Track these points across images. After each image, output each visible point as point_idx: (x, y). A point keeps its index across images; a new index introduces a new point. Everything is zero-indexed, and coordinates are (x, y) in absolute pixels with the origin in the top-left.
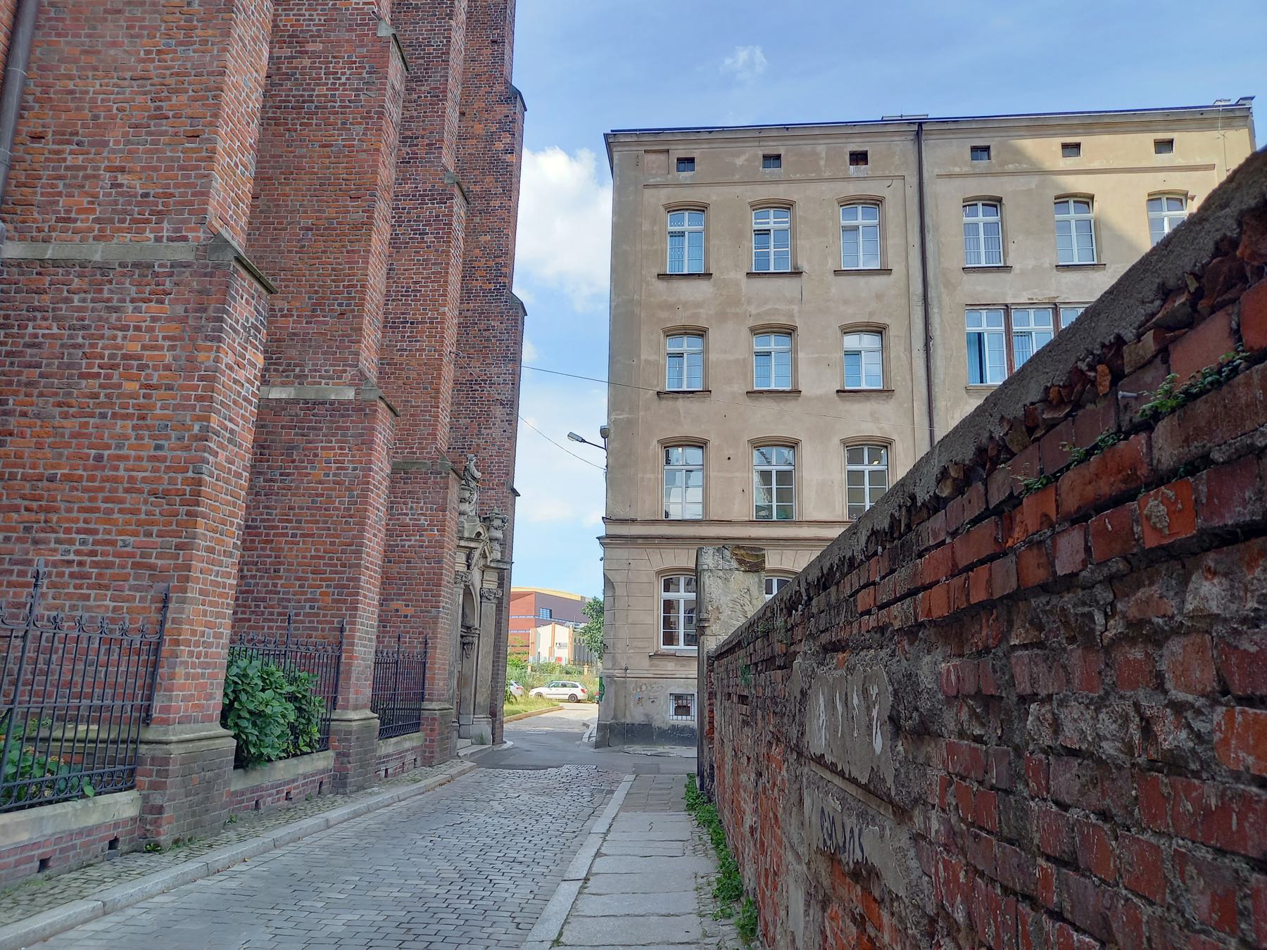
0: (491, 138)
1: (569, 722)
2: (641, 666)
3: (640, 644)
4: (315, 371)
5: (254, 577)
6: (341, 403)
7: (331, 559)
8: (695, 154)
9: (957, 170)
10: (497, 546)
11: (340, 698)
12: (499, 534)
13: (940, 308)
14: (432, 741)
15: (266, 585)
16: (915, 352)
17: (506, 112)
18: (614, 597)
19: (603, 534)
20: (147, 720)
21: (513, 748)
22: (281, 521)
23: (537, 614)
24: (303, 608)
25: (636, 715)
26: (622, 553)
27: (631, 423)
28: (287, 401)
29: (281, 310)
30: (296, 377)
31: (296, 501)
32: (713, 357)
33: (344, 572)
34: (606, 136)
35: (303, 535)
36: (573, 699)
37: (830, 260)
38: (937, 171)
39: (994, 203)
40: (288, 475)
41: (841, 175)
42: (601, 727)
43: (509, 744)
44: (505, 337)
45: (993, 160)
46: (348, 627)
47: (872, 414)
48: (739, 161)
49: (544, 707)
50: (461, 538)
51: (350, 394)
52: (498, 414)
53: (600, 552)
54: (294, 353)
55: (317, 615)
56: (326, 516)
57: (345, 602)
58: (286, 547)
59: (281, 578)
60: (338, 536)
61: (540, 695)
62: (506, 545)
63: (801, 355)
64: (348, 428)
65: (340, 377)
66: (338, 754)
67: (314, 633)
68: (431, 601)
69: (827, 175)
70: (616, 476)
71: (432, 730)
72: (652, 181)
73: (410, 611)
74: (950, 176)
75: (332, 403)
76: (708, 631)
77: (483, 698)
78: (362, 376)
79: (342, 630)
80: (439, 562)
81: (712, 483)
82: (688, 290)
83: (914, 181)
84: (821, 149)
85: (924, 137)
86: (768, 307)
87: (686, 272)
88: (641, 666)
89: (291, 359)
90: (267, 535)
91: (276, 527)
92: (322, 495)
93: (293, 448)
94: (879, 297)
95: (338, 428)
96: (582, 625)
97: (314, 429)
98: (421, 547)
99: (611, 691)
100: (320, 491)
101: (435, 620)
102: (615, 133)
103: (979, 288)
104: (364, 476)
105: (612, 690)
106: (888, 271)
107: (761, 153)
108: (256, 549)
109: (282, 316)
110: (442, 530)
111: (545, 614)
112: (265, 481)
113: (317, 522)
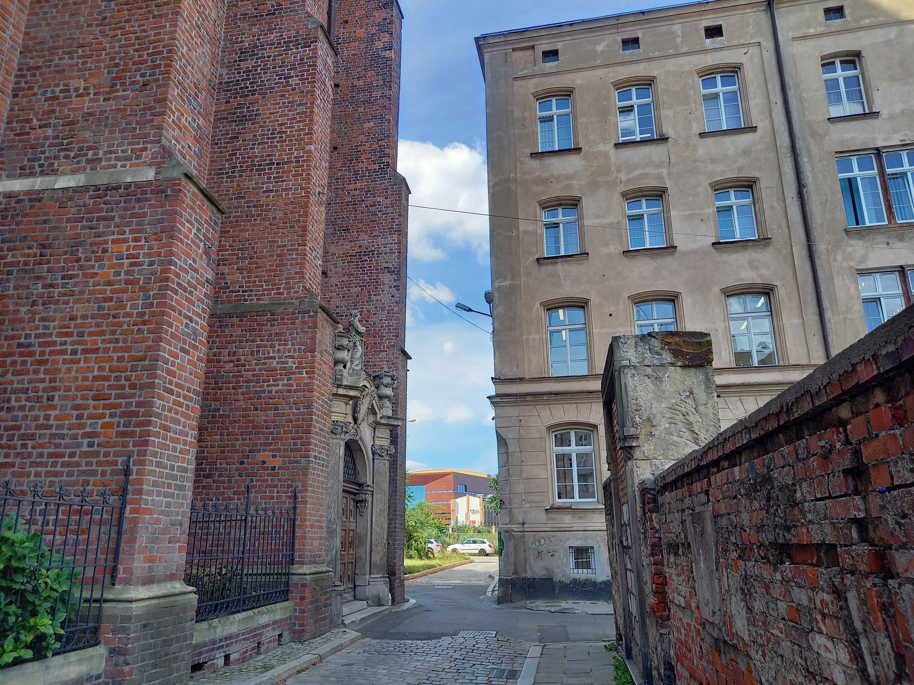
0: (371, 39)
1: (476, 575)
2: (537, 518)
3: (535, 498)
4: (111, 152)
5: (22, 408)
6: (138, 185)
7: (118, 379)
8: (559, 46)
9: (812, 31)
10: (387, 404)
11: (121, 568)
12: (389, 392)
13: (810, 157)
14: (302, 611)
15: (36, 418)
16: (788, 201)
17: (385, 16)
18: (507, 453)
19: (494, 393)
20: (292, 562)
21: (415, 607)
22: (60, 335)
24: (79, 445)
25: (536, 569)
26: (512, 411)
28: (75, 190)
29: (77, 90)
30: (89, 161)
31: (79, 309)
32: (588, 222)
33: (133, 396)
34: (477, 40)
35: (85, 351)
36: (483, 553)
37: (694, 125)
38: (792, 34)
39: (852, 59)
40: (71, 277)
41: (698, 48)
43: (413, 601)
44: (390, 210)
45: (848, 18)
46: (134, 469)
47: (750, 262)
48: (600, 48)
49: (457, 560)
50: (339, 386)
51: (150, 174)
52: (386, 281)
53: (490, 412)
54: (88, 134)
55: (97, 454)
56: (114, 324)
57: (132, 434)
58: (64, 367)
59: (54, 408)
60: (127, 349)
61: (454, 550)
62: (399, 403)
63: (673, 213)
64: (145, 215)
65: (139, 157)
66: (112, 651)
67: (92, 479)
68: (300, 450)
69: (684, 49)
70: (505, 342)
71: (302, 598)
72: (520, 74)
73: (278, 462)
74: (805, 37)
75: (128, 186)
76: (637, 454)
77: (379, 556)
78: (167, 153)
79: (127, 472)
80: (309, 406)
82: (560, 165)
83: (769, 45)
84: (677, 28)
85: (775, 6)
86: (635, 174)
87: (557, 149)
89: (84, 141)
90: (42, 353)
91: (54, 343)
92: (110, 299)
93: (78, 244)
94: (746, 153)
95: (133, 216)
96: (489, 496)
97: (104, 219)
98: (289, 391)
100: (108, 294)
101: (305, 471)
102: (484, 37)
103: (847, 136)
104: (163, 271)
105: (511, 544)
106: (753, 129)
107: (619, 38)
108: (27, 372)
109: (77, 96)
110: (311, 373)
111: (461, 488)
112: (44, 287)
113: (103, 333)
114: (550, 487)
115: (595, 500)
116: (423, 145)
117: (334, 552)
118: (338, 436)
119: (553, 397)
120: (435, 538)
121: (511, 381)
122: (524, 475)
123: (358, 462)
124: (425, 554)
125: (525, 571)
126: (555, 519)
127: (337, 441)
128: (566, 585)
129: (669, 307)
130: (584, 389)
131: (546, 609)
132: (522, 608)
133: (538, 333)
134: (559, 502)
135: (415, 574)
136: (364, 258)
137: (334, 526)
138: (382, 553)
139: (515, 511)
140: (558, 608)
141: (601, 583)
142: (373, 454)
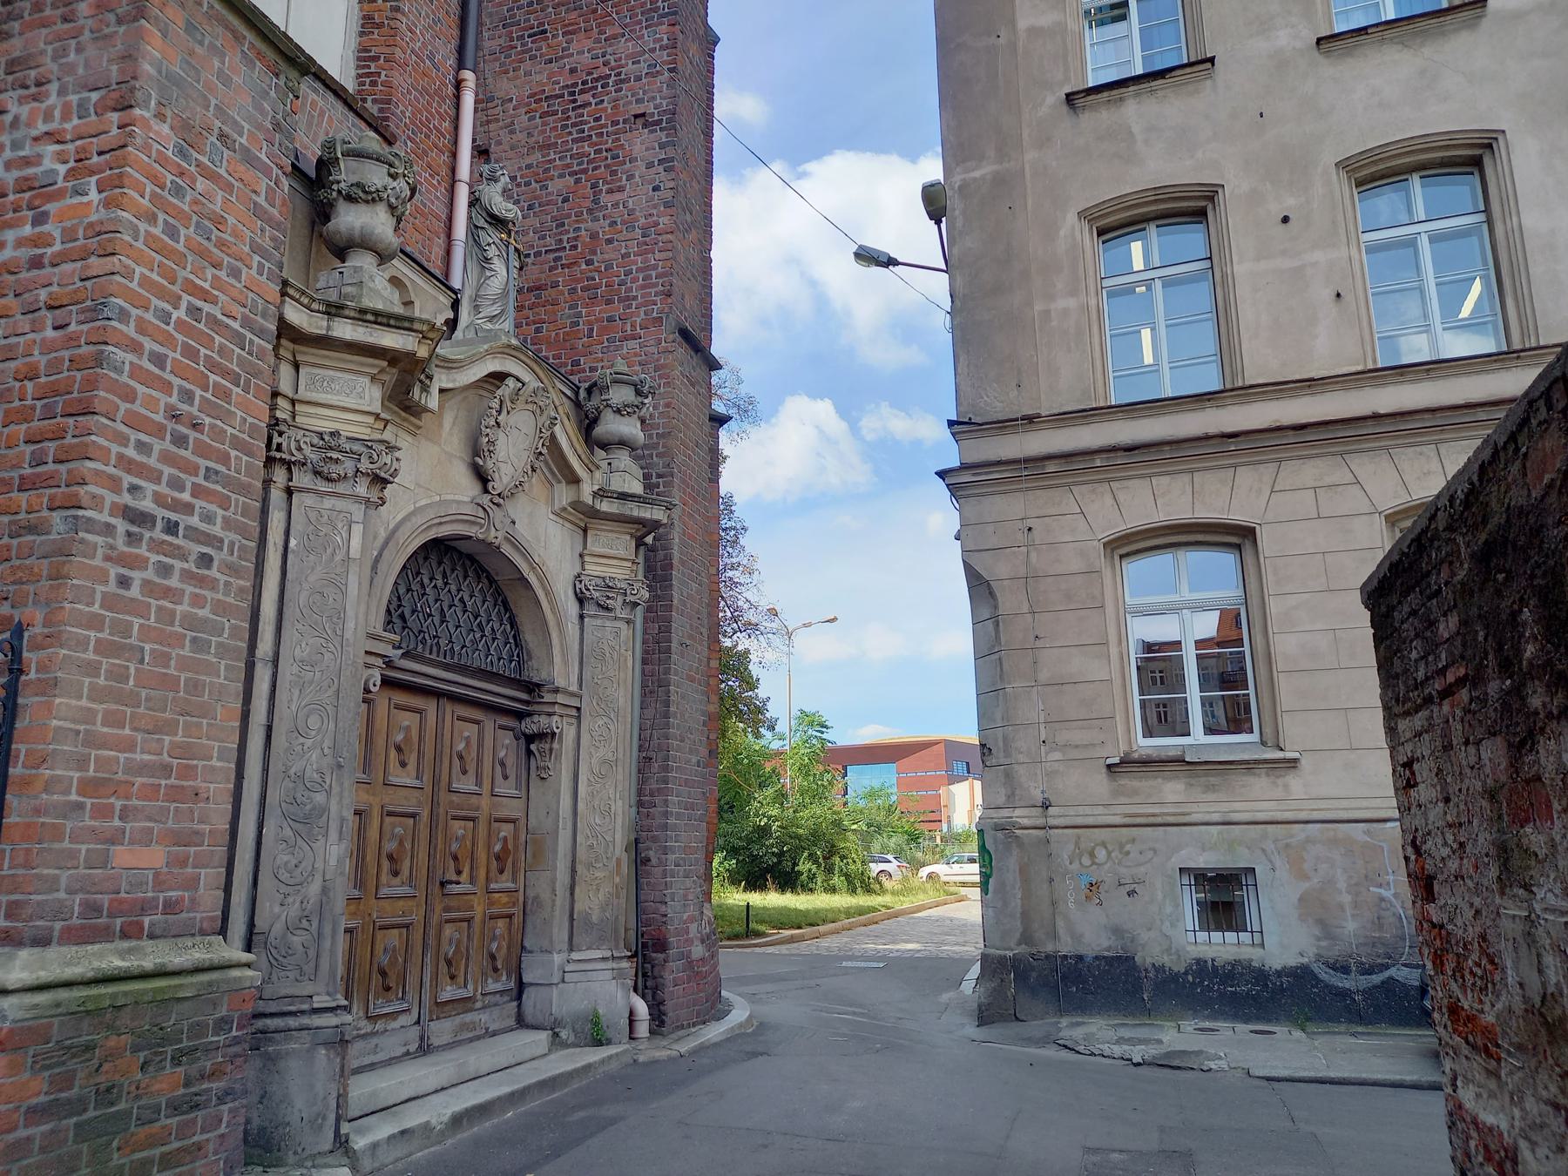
2: (1085, 791)
3: (1077, 736)
18: (995, 620)
23: (949, 769)
25: (1086, 931)
26: (1008, 507)
27: (1001, 182)
42: (992, 966)
43: (739, 1014)
49: (930, 896)
68: (49, 481)
77: (603, 894)
80: (94, 313)
81: (1243, 291)
88: (1085, 791)
99: (1010, 865)
105: (1012, 862)
111: (960, 768)
114: (1119, 705)
115: (1254, 737)
116: (883, 157)
117: (314, 888)
118: (341, 488)
119: (1121, 458)
120: (895, 852)
121: (1003, 425)
122: (1044, 676)
123: (524, 620)
124: (861, 883)
125: (1054, 936)
126: (1136, 792)
127: (340, 504)
128: (1174, 977)
129: (1462, 190)
130: (1212, 430)
131: (1117, 1050)
132: (1043, 1041)
133: (1073, 293)
134: (1147, 745)
135: (821, 928)
136: (581, 99)
137: (319, 798)
138: (606, 889)
139: (1021, 771)
140: (1152, 1051)
141: (1279, 973)
142: (581, 600)
